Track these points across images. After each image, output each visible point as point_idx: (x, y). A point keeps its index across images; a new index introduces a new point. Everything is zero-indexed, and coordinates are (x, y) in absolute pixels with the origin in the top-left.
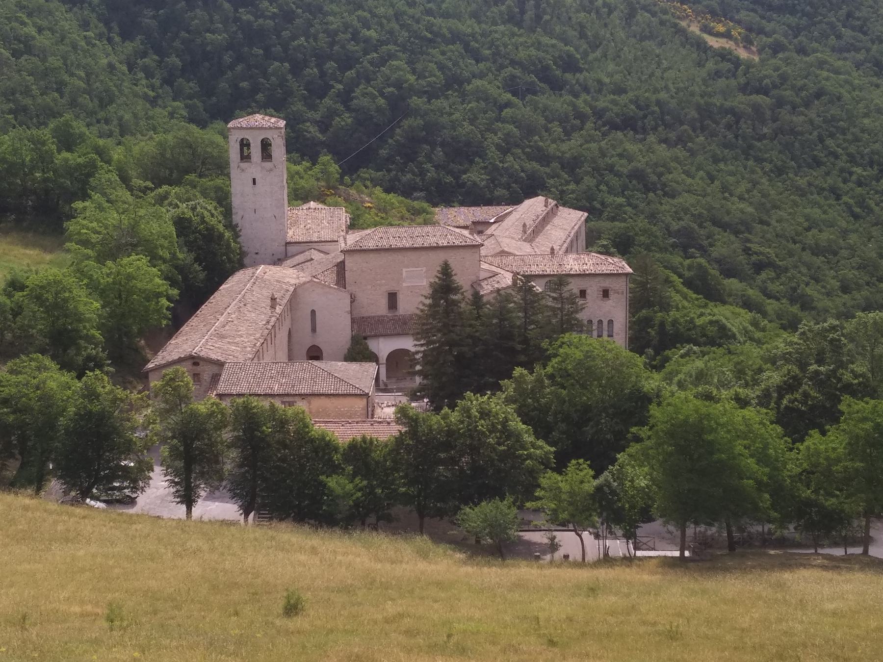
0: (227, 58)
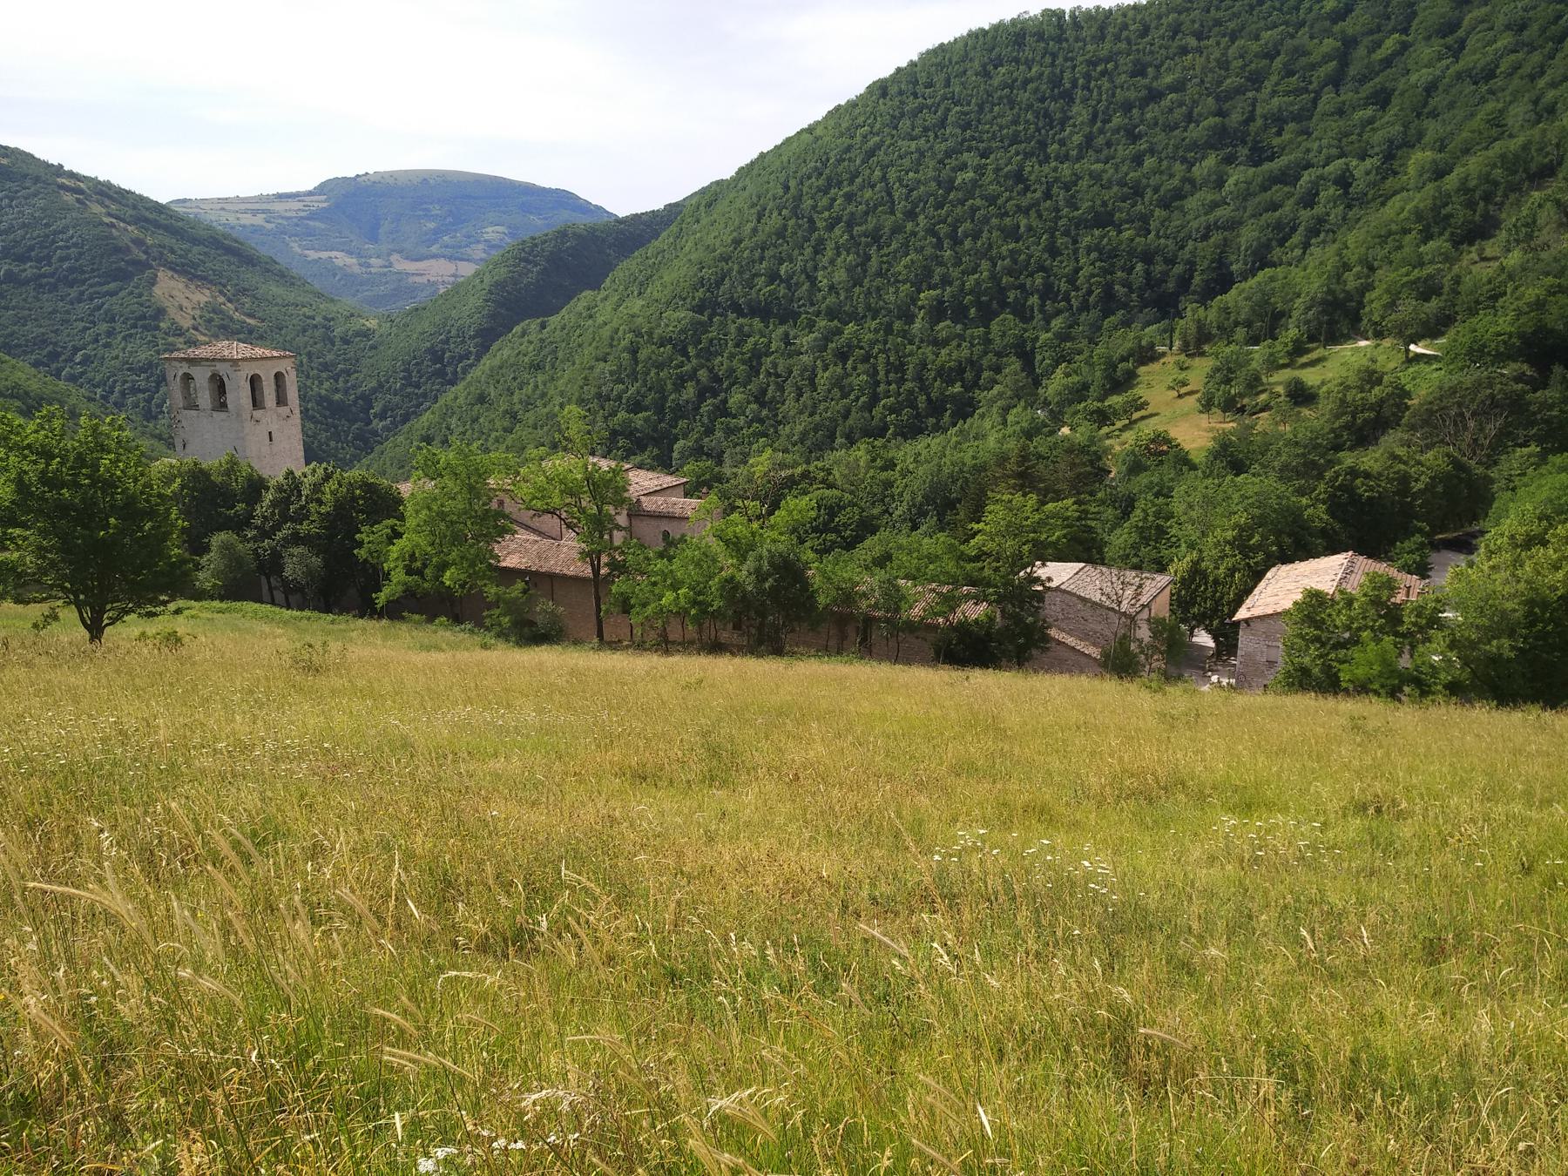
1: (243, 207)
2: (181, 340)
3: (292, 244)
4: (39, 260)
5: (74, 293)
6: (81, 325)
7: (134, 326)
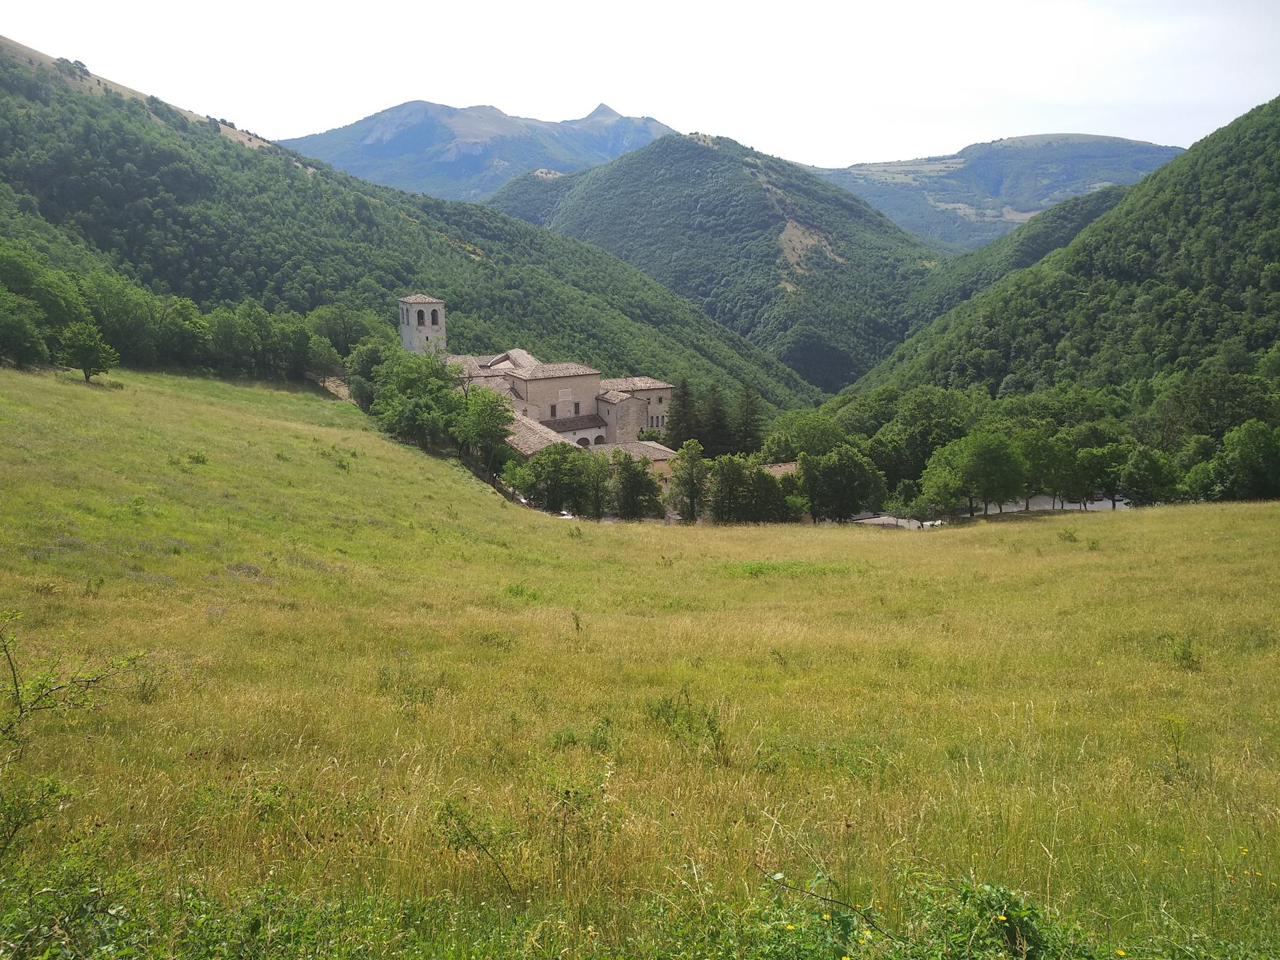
0: (186, 264)
1: (900, 169)
2: (786, 272)
3: (928, 198)
4: (719, 214)
5: (733, 237)
6: (731, 259)
7: (761, 261)
